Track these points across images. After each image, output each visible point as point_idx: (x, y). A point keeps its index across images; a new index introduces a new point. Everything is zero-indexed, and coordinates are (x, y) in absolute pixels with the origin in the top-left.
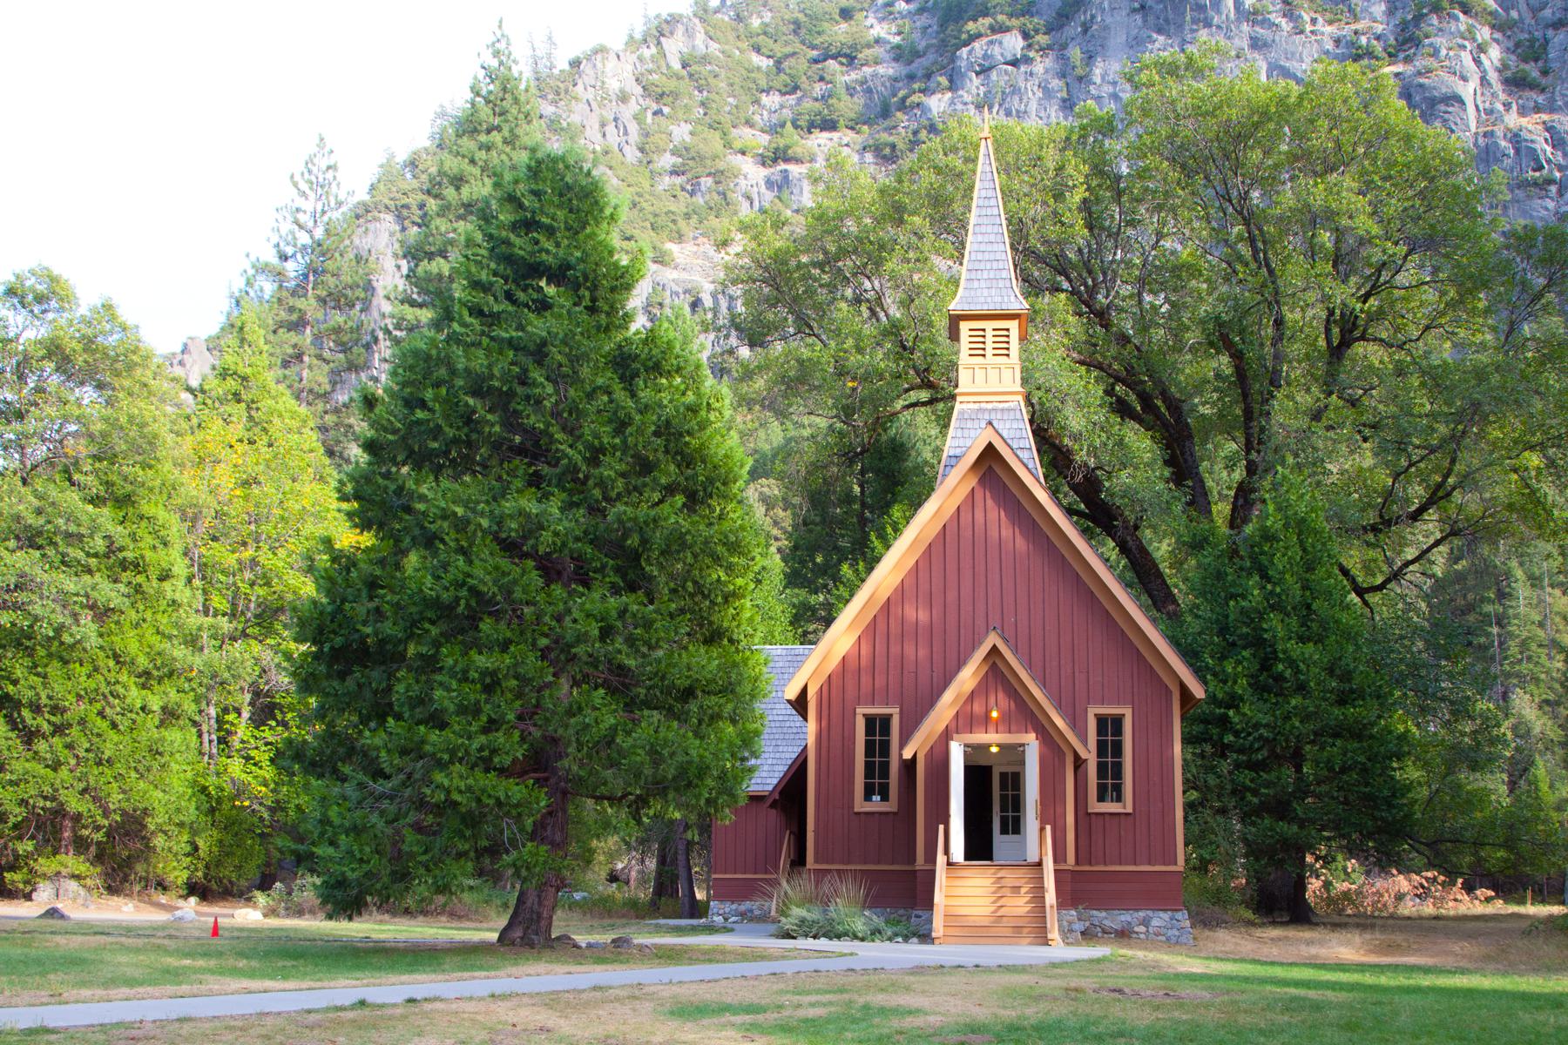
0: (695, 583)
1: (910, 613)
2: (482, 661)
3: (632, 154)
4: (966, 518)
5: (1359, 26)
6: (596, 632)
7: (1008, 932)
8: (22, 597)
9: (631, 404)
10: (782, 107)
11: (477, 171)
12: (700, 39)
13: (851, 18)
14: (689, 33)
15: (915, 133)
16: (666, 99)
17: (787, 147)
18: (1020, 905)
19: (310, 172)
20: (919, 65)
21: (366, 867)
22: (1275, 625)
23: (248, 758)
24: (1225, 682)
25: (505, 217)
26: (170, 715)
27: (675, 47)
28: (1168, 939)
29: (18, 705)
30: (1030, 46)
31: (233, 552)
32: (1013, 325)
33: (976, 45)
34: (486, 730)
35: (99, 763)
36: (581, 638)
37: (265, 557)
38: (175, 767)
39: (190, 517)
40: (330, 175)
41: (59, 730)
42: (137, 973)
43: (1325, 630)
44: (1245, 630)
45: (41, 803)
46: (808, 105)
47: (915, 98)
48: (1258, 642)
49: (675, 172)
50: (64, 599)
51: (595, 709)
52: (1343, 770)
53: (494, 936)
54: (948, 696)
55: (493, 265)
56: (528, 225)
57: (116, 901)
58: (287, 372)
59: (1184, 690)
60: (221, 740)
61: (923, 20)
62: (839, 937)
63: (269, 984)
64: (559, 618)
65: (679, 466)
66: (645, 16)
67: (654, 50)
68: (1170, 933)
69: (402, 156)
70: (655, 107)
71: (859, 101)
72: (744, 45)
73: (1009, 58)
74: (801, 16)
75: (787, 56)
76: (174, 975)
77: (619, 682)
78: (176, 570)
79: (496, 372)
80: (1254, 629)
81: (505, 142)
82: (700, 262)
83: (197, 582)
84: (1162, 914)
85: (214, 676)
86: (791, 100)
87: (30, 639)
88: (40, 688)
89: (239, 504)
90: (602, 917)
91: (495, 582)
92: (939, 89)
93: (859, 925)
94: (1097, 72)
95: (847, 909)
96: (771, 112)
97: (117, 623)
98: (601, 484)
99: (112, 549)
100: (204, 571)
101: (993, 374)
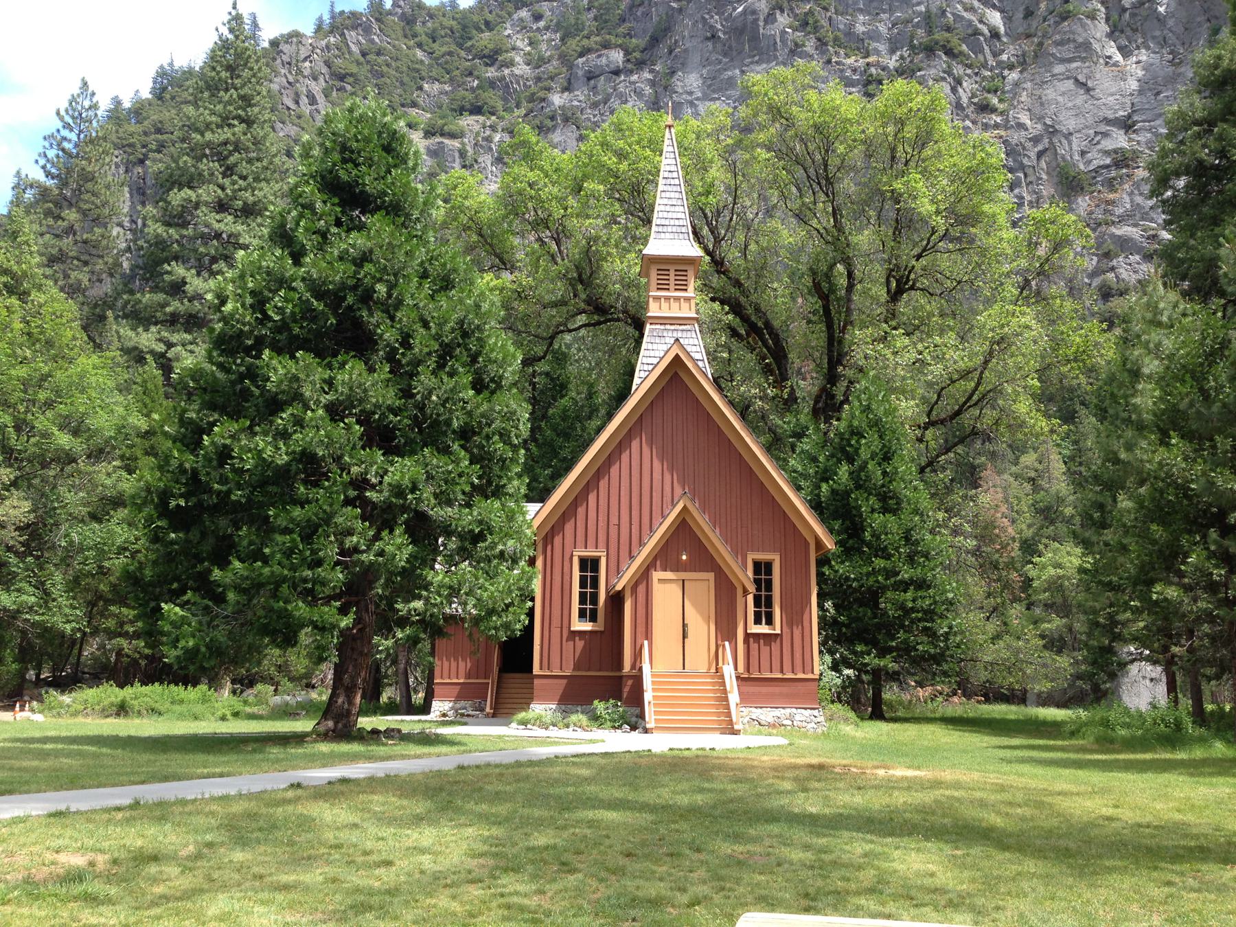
5: (870, 59)
19: (74, 110)
40: (91, 113)
59: (819, 544)
66: (332, 11)
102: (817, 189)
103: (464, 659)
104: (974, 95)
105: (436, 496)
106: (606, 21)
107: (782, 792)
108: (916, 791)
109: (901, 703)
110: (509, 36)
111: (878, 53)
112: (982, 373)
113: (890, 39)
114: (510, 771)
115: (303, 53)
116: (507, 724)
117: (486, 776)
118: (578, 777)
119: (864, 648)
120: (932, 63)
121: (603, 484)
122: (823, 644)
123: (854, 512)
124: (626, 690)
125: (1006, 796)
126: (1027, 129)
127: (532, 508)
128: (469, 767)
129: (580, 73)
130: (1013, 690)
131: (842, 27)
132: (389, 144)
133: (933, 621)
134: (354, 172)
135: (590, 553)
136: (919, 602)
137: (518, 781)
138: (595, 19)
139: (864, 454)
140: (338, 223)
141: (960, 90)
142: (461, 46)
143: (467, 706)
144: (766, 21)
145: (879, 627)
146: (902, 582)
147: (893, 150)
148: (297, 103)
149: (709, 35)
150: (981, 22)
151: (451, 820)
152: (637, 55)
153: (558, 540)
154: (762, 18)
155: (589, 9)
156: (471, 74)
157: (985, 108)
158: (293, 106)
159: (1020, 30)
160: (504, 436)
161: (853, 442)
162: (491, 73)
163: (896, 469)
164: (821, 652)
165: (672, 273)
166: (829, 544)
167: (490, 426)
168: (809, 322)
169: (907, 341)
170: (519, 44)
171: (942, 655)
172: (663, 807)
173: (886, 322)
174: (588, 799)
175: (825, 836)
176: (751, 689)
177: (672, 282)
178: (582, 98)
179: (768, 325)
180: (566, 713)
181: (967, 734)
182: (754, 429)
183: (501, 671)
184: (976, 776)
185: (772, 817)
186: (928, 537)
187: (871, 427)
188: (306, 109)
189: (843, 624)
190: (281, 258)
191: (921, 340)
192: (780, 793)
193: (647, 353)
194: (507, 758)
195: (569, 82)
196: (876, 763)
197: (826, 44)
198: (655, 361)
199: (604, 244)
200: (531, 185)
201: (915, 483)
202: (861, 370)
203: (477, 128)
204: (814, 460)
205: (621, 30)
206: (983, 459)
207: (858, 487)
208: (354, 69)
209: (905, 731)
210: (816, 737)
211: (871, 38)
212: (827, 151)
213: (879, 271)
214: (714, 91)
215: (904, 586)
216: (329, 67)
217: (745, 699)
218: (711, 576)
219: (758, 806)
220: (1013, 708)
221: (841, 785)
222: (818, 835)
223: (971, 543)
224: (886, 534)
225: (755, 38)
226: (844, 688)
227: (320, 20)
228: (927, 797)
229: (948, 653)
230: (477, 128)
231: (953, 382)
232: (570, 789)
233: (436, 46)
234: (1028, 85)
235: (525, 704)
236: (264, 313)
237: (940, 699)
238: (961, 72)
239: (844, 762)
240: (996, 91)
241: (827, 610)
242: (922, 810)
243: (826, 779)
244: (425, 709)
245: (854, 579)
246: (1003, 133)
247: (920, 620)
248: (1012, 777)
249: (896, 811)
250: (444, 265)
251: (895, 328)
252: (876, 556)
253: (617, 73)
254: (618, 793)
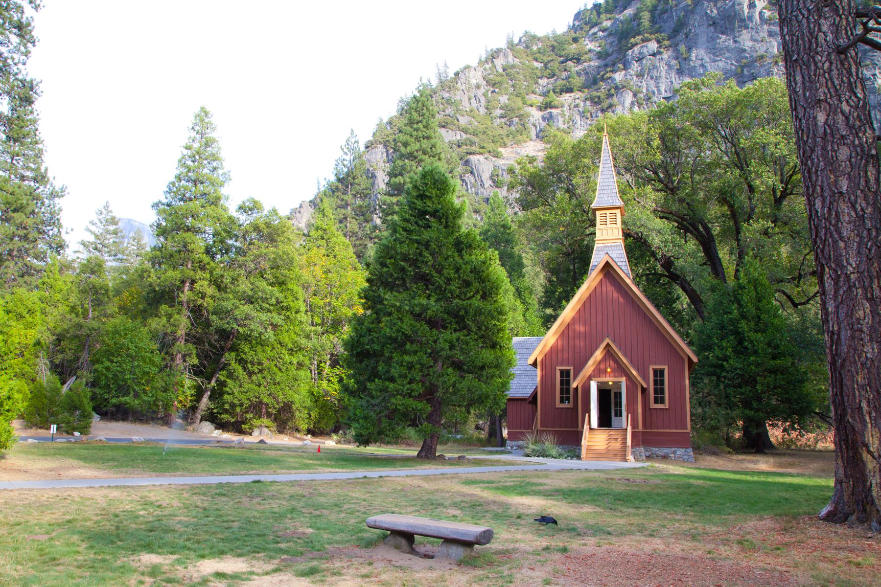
0: (485, 326)
1: (577, 327)
2: (407, 358)
3: (483, 111)
4: (598, 290)
6: (448, 347)
7: (612, 456)
8: (247, 322)
9: (461, 261)
10: (548, 84)
11: (413, 140)
12: (510, 58)
13: (578, 42)
14: (506, 56)
15: (609, 90)
16: (496, 86)
17: (551, 102)
18: (617, 445)
20: (609, 60)
21: (369, 431)
22: (743, 325)
23: (329, 381)
24: (722, 350)
25: (415, 194)
26: (300, 365)
27: (499, 62)
28: (684, 460)
29: (246, 362)
30: (660, 47)
31: (322, 300)
32: (618, 212)
33: (635, 48)
34: (409, 383)
35: (275, 384)
36: (442, 349)
37: (334, 302)
38: (302, 385)
39: (306, 287)
40: (356, 145)
41: (261, 371)
42: (296, 465)
43: (767, 326)
44: (731, 327)
45: (254, 399)
46: (559, 82)
47: (608, 75)
48: (737, 333)
49: (502, 117)
50: (262, 323)
51: (448, 375)
52: (775, 388)
53: (416, 453)
54: (591, 362)
55: (410, 212)
56: (422, 197)
57: (282, 436)
58: (341, 225)
59: (690, 359)
60: (319, 373)
61: (610, 40)
62: (547, 457)
63: (337, 470)
64: (435, 342)
65: (479, 283)
67: (490, 65)
68: (684, 457)
69: (385, 120)
70: (492, 89)
71: (583, 78)
72: (530, 58)
73: (651, 53)
74: (555, 43)
75: (549, 62)
76: (308, 466)
77: (458, 366)
78: (301, 309)
79: (411, 252)
80: (735, 327)
81: (424, 127)
82: (514, 155)
83: (309, 313)
84: (681, 449)
85: (316, 350)
86: (552, 80)
87: (250, 337)
88: (254, 356)
89: (324, 281)
90: (467, 445)
91: (411, 330)
92: (619, 70)
93: (554, 453)
94: (693, 55)
95: (549, 445)
96: (543, 87)
97: (281, 330)
98: (451, 292)
99: (278, 302)
100: (311, 308)
101: (610, 232)
149: (711, 23)
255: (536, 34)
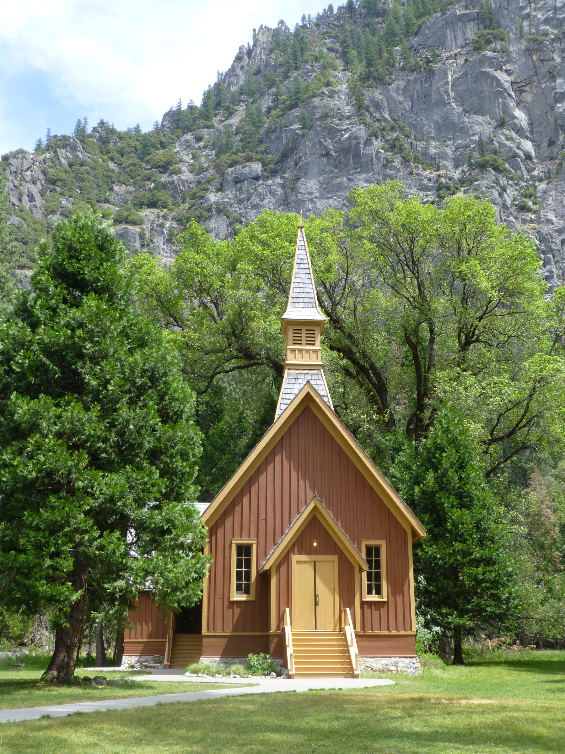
5: (441, 172)
59: (414, 533)
66: (48, 135)
84: (405, 659)
102: (406, 268)
103: (147, 624)
104: (515, 200)
105: (135, 501)
106: (249, 143)
107: (394, 718)
108: (488, 714)
109: (475, 652)
110: (177, 152)
111: (446, 168)
112: (528, 403)
113: (454, 159)
114: (196, 707)
115: (26, 165)
116: (183, 673)
117: (180, 710)
118: (246, 710)
119: (448, 611)
120: (485, 176)
121: (254, 489)
122: (418, 608)
123: (439, 508)
124: (272, 646)
125: (551, 715)
126: (553, 224)
127: (201, 507)
128: (166, 704)
129: (230, 179)
130: (557, 639)
131: (419, 149)
132: (103, 244)
133: (498, 589)
134: (77, 265)
135: (245, 541)
136: (487, 575)
137: (203, 714)
138: (241, 140)
139: (445, 464)
140: (65, 301)
141: (505, 195)
142: (142, 159)
143: (149, 660)
144: (365, 145)
145: (459, 594)
146: (475, 560)
147: (459, 243)
148: (20, 200)
149: (324, 153)
150: (518, 148)
151: (162, 741)
152: (272, 166)
153: (220, 532)
154: (362, 142)
155: (237, 134)
156: (149, 179)
157: (523, 208)
158: (17, 203)
159: (546, 154)
160: (184, 456)
161: (437, 455)
162: (164, 178)
163: (469, 475)
164: (417, 614)
165: (304, 332)
166: (422, 533)
167: (173, 448)
168: (403, 365)
169: (473, 379)
170: (185, 158)
171: (505, 614)
172: (311, 730)
173: (459, 366)
174: (256, 725)
175: (427, 746)
176: (367, 643)
177: (304, 339)
178: (231, 196)
179: (372, 366)
180: (228, 664)
181: (523, 673)
182: (363, 443)
183: (175, 632)
184: (529, 702)
185: (389, 735)
186: (493, 526)
187: (450, 444)
188: (26, 204)
189: (432, 593)
190: (23, 328)
191: (485, 379)
192: (393, 718)
193: (287, 391)
194: (192, 697)
195: (222, 186)
196: (459, 696)
197: (408, 161)
198: (292, 397)
199: (252, 308)
200: (197, 265)
201: (483, 485)
202: (441, 401)
203: (153, 217)
204: (409, 468)
205: (260, 149)
206: (532, 464)
207: (441, 489)
208: (63, 176)
209: (479, 672)
210: (415, 679)
211: (440, 157)
212: (412, 242)
213: (452, 327)
214: (328, 192)
215: (476, 563)
216: (45, 175)
217: (362, 651)
218: (335, 558)
219: (379, 728)
220: (557, 652)
221: (436, 712)
222: (422, 746)
223: (524, 530)
224: (463, 524)
225: (357, 156)
226: (434, 641)
227: (40, 142)
228: (496, 718)
229: (508, 613)
230: (153, 217)
231: (508, 410)
232: (243, 719)
233: (124, 159)
234: (553, 193)
235: (195, 658)
236: (10, 367)
237: (504, 648)
238: (505, 182)
239: (437, 696)
240: (530, 197)
241: (420, 582)
242: (493, 726)
243: (425, 708)
244: (116, 662)
245: (440, 559)
246: (536, 226)
247: (488, 588)
248: (554, 702)
249: (475, 727)
250: (140, 330)
251: (465, 370)
252: (456, 541)
253: (257, 178)
254: (277, 721)
255: (115, 127)
